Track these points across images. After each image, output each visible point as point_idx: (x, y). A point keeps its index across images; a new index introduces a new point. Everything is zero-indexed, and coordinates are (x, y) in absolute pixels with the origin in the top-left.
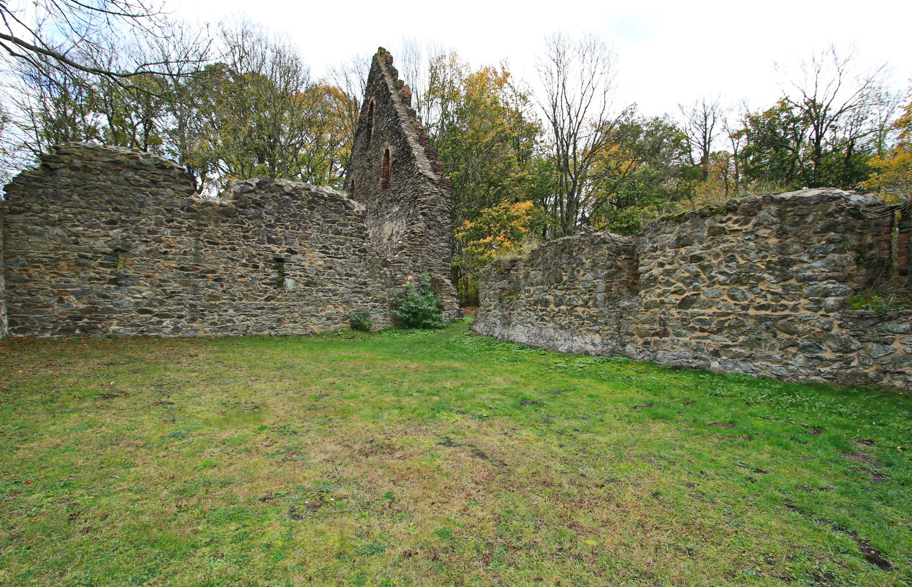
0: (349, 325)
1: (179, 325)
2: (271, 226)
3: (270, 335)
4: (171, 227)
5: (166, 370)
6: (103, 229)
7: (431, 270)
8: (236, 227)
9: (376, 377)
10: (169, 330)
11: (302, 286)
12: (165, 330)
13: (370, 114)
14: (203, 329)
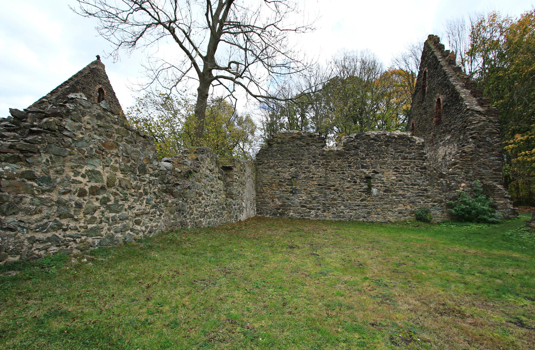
0: (414, 218)
1: (318, 214)
2: (364, 159)
3: (364, 221)
4: (315, 165)
5: (314, 236)
6: (288, 168)
7: (482, 179)
8: (345, 161)
9: (441, 256)
10: (314, 216)
11: (382, 193)
12: (312, 216)
13: (424, 79)
14: (329, 216)
